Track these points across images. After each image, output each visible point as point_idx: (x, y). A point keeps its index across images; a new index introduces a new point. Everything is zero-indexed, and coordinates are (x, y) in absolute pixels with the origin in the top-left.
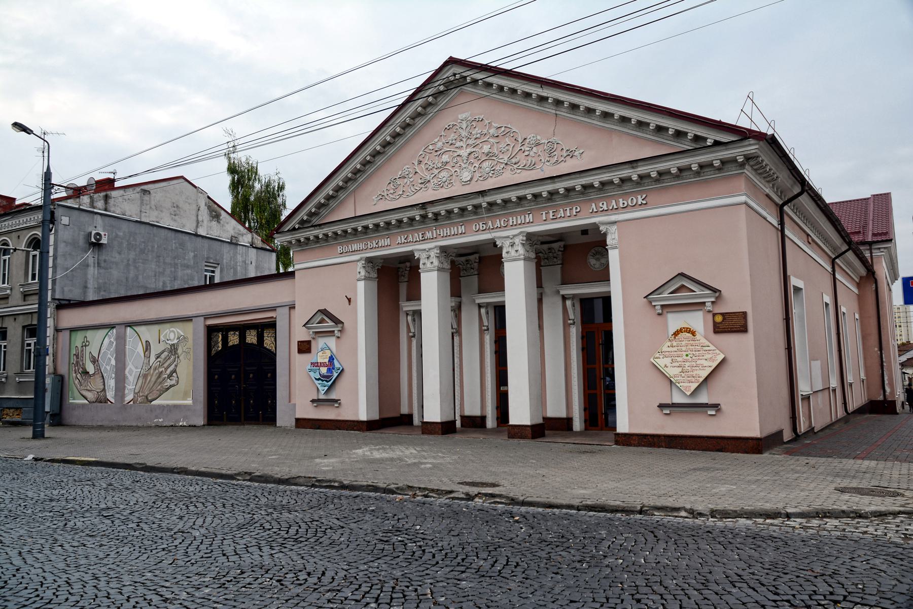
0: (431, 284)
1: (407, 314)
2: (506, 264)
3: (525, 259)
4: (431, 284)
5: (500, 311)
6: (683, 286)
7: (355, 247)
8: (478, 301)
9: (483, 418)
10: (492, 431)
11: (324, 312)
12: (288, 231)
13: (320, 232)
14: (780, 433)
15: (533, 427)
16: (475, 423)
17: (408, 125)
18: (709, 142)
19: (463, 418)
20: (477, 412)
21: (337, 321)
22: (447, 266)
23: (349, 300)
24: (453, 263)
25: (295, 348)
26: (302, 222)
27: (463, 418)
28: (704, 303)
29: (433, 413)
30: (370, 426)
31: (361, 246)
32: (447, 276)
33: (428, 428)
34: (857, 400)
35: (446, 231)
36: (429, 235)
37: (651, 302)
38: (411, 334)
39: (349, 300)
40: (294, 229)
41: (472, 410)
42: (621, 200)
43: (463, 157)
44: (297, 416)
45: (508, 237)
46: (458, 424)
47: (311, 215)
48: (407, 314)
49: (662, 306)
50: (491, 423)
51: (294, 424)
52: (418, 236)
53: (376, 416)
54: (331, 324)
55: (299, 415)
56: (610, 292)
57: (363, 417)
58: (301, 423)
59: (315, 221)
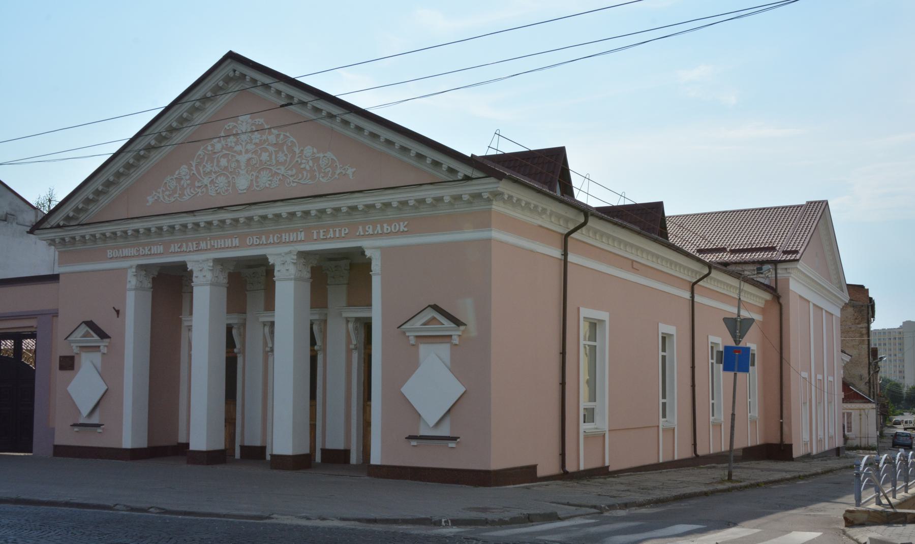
0: (289, 293)
1: (265, 325)
2: (278, 284)
3: (296, 279)
4: (289, 293)
5: (366, 326)
6: (434, 318)
7: (126, 252)
8: (345, 315)
9: (346, 453)
10: (356, 467)
11: (91, 324)
12: (51, 228)
13: (87, 231)
14: (534, 468)
15: (133, 451)
16: (336, 458)
17: (186, 120)
18: (460, 176)
19: (324, 451)
20: (341, 446)
21: (103, 335)
22: (307, 274)
23: (118, 312)
24: (231, 276)
25: (56, 363)
26: (68, 218)
27: (324, 451)
28: (451, 336)
29: (284, 441)
30: (135, 454)
31: (133, 251)
32: (307, 287)
33: (281, 462)
34: (749, 437)
35: (221, 243)
36: (203, 245)
37: (404, 333)
38: (268, 349)
39: (118, 312)
40: (58, 226)
41: (336, 443)
42: (385, 225)
43: (246, 160)
44: (56, 443)
45: (280, 254)
46: (318, 458)
47: (77, 210)
48: (265, 325)
49: (417, 337)
50: (354, 459)
51: (51, 452)
52: (192, 246)
53: (143, 444)
54: (96, 337)
55: (59, 441)
56: (370, 318)
57: (127, 443)
58: (62, 451)
59: (83, 218)
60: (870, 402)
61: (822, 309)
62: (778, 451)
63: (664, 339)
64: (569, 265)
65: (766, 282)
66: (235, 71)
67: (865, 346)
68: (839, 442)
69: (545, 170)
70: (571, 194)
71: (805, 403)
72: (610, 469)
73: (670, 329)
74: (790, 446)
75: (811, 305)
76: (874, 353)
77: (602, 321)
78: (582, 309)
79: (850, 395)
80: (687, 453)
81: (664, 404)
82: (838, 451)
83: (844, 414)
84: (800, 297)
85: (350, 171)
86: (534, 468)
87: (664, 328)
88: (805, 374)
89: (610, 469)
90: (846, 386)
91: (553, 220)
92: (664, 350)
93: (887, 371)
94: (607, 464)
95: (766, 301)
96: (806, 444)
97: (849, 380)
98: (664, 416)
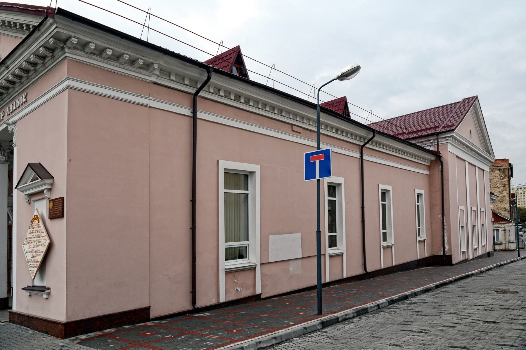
14: (147, 310)
60: (511, 222)
61: (475, 166)
62: (441, 260)
63: (418, 196)
64: (364, 161)
65: (432, 148)
67: (507, 191)
68: (490, 249)
69: (339, 109)
70: (246, 75)
71: (462, 227)
72: (263, 297)
73: (421, 191)
74: (450, 256)
75: (467, 163)
76: (513, 196)
77: (252, 173)
78: (221, 162)
79: (497, 218)
80: (359, 271)
81: (419, 229)
82: (489, 254)
83: (494, 230)
84: (457, 157)
86: (147, 310)
87: (418, 191)
88: (462, 207)
89: (263, 297)
90: (495, 215)
91: (305, 121)
92: (418, 202)
93: (521, 204)
94: (258, 292)
95: (431, 161)
96: (464, 253)
97: (497, 211)
98: (419, 235)
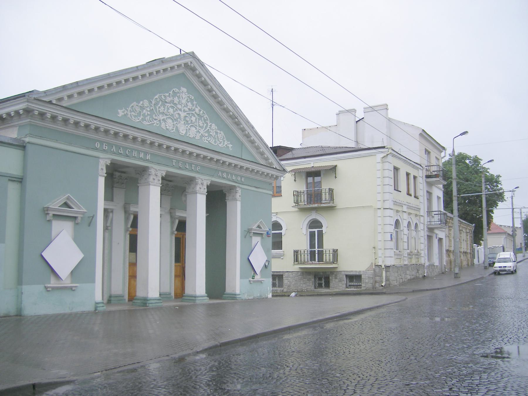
66: (191, 63)
85: (230, 146)
